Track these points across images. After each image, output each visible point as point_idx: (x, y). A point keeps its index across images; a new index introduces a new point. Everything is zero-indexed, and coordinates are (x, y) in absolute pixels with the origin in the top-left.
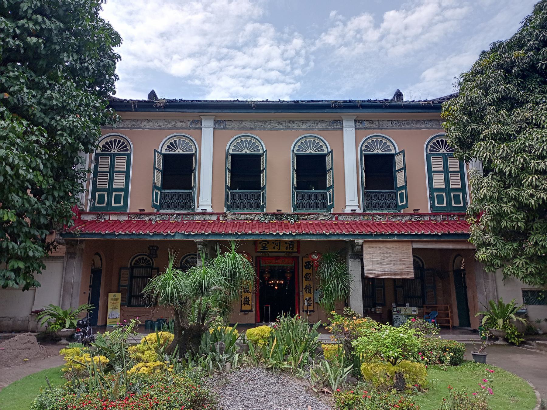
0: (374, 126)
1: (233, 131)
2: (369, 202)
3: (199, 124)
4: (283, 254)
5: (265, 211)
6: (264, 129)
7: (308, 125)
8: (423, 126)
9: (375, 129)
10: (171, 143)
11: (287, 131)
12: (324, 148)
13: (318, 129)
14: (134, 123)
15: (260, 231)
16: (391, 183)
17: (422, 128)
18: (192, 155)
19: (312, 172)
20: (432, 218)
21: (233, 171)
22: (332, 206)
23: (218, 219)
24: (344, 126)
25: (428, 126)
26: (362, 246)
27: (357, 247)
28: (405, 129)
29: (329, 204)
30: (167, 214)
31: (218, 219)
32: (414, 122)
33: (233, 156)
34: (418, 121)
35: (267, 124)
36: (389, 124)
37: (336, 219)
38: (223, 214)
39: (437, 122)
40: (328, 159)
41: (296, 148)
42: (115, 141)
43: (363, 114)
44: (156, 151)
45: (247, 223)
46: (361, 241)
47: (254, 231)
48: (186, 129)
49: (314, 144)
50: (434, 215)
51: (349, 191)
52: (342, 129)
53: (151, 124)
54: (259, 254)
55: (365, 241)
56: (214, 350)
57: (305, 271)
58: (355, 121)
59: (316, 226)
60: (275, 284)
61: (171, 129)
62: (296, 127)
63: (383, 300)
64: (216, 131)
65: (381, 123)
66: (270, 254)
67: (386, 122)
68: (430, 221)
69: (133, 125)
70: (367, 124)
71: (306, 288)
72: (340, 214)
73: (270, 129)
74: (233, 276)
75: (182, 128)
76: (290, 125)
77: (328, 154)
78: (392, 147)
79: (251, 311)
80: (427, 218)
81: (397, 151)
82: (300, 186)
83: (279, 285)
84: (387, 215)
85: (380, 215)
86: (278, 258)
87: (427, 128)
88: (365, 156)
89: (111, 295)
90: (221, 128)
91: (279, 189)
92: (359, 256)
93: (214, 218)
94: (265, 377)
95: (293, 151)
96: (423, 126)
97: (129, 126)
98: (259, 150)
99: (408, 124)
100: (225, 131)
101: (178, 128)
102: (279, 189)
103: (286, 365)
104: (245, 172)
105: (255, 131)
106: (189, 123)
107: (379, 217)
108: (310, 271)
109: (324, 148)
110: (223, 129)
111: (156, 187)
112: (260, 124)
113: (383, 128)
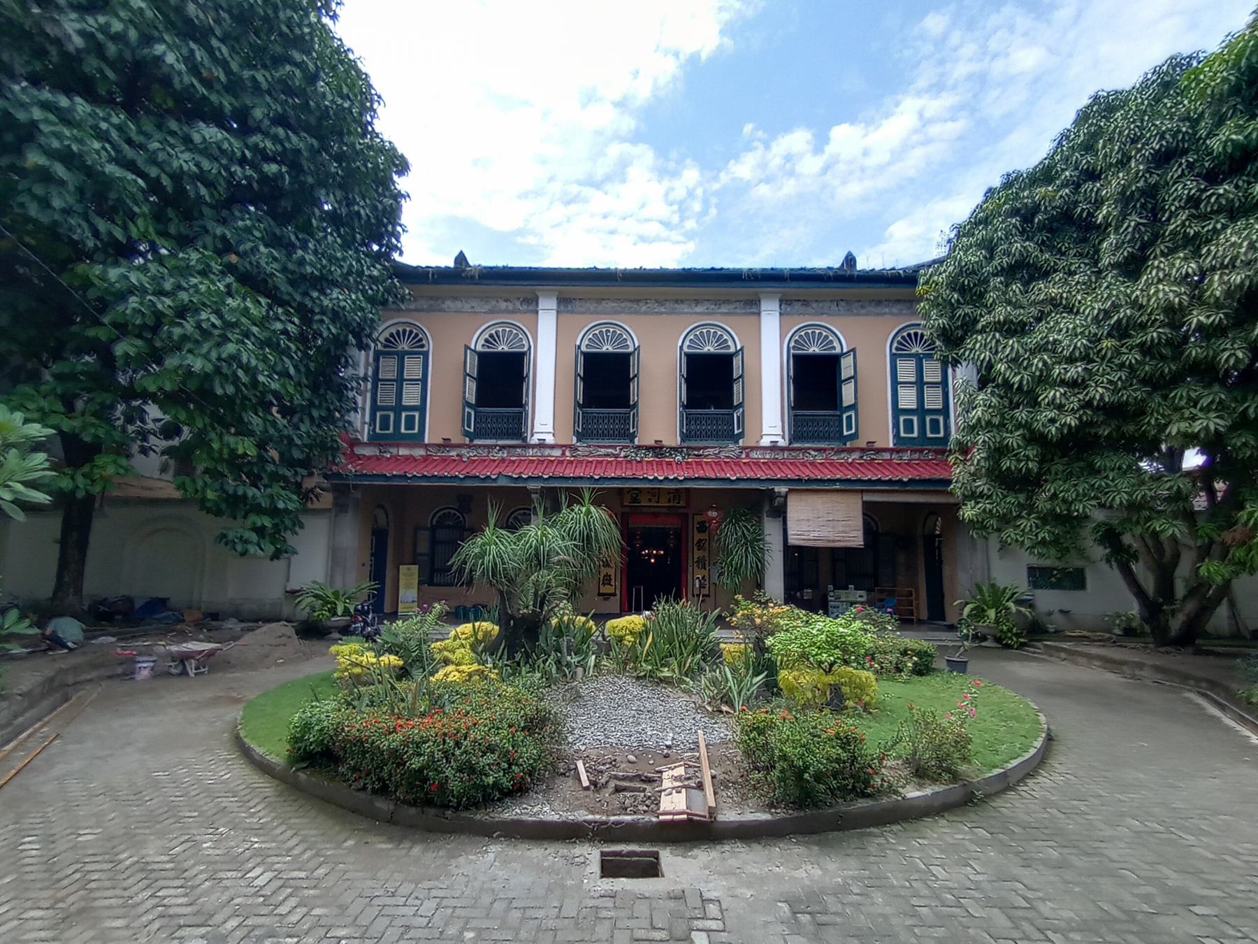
4: (664, 510)
15: (629, 474)
18: (523, 354)
19: (712, 382)
22: (741, 435)
23: (563, 454)
24: (763, 308)
25: (895, 310)
29: (845, 433)
36: (834, 307)
37: (747, 456)
41: (586, 342)
43: (792, 290)
46: (783, 489)
47: (618, 473)
48: (515, 311)
53: (458, 304)
54: (627, 510)
56: (558, 649)
59: (716, 465)
60: (650, 556)
66: (644, 510)
73: (646, 313)
74: (587, 540)
79: (614, 595)
80: (887, 456)
83: (656, 557)
86: (656, 515)
91: (659, 408)
93: (557, 453)
94: (635, 689)
98: (834, 348)
99: (862, 307)
102: (659, 408)
103: (666, 673)
112: (629, 304)
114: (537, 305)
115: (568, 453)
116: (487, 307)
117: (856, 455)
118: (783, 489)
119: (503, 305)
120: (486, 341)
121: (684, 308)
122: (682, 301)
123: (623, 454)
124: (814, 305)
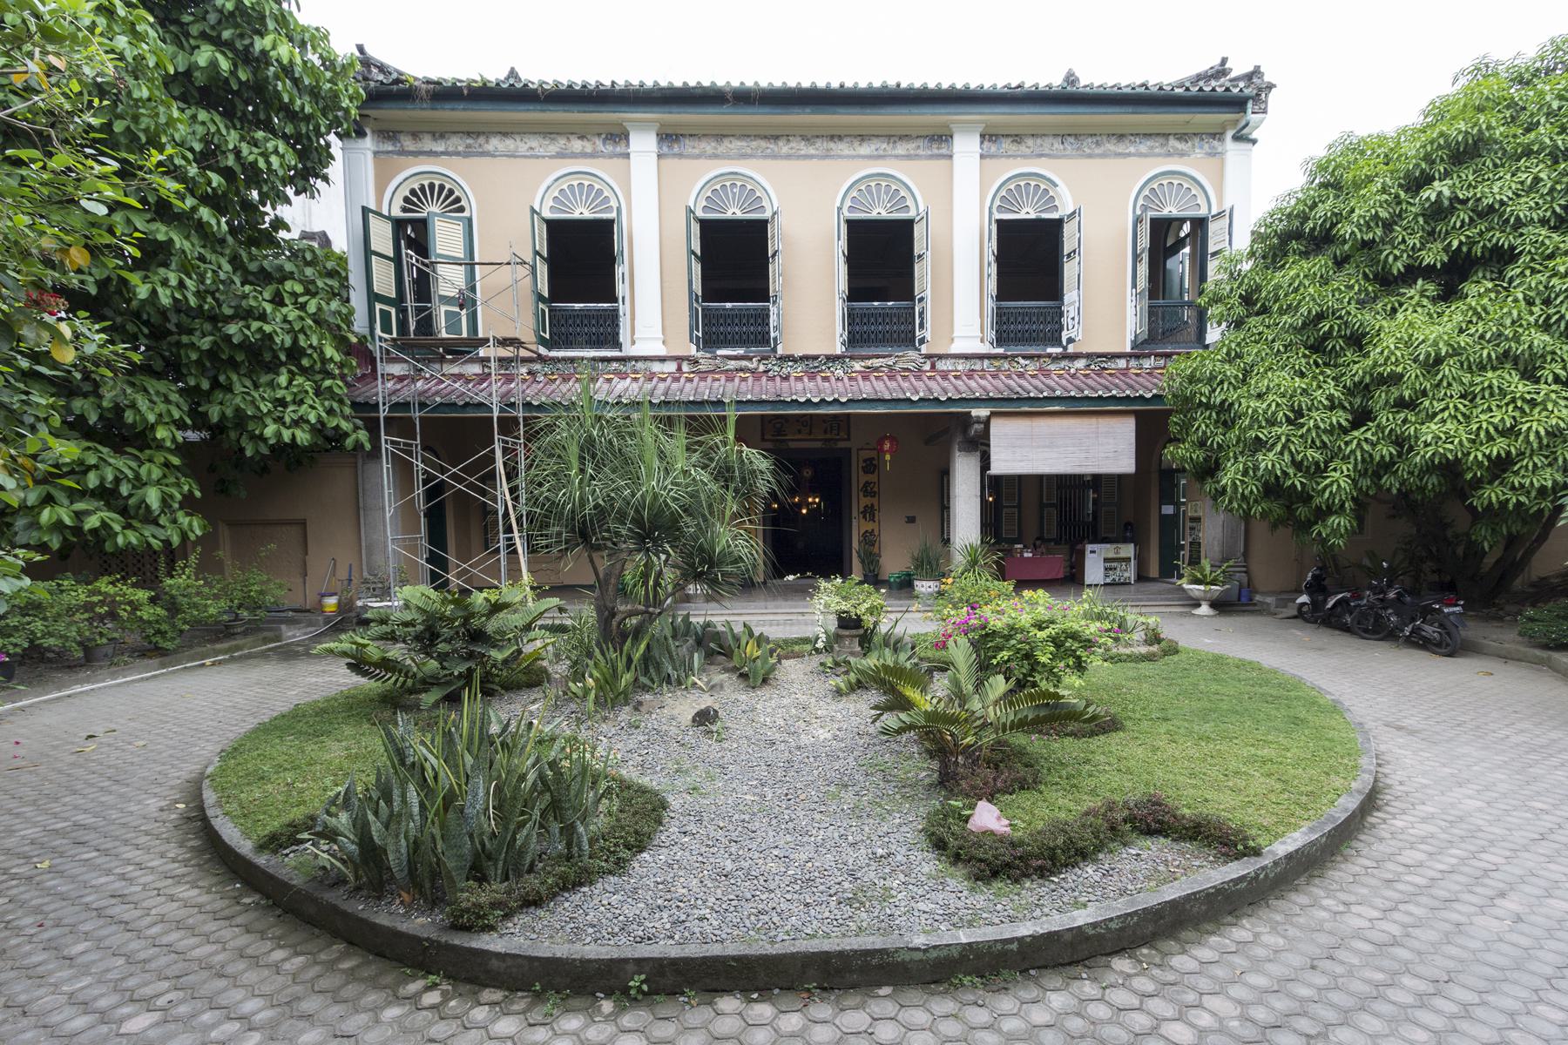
0: (1023, 148)
1: (702, 162)
2: (1009, 330)
3: (623, 143)
5: (780, 351)
6: (774, 157)
7: (873, 147)
8: (1132, 149)
9: (1024, 156)
10: (413, 192)
11: (827, 162)
12: (910, 202)
13: (897, 157)
14: (470, 141)
16: (1052, 288)
17: (1129, 155)
19: (882, 258)
20: (1133, 363)
21: (554, 262)
23: (679, 369)
26: (987, 422)
27: (976, 426)
28: (1090, 156)
30: (564, 359)
31: (679, 369)
32: (1113, 140)
33: (704, 224)
34: (1121, 137)
35: (780, 144)
36: (1057, 145)
37: (933, 366)
38: (687, 358)
39: (1161, 140)
40: (1068, 230)
41: (848, 203)
42: (432, 186)
44: (533, 211)
45: (737, 382)
46: (981, 412)
48: (593, 155)
49: (886, 193)
50: (1137, 357)
51: (958, 301)
52: (951, 157)
55: (993, 414)
57: (864, 478)
58: (982, 136)
61: (561, 155)
62: (846, 152)
63: (1047, 526)
64: (663, 162)
65: (1039, 141)
67: (1050, 140)
68: (1128, 369)
69: (469, 146)
70: (1006, 145)
71: (864, 513)
72: (940, 357)
73: (788, 157)
75: (584, 155)
76: (832, 145)
77: (1220, 215)
78: (1201, 200)
80: (1122, 363)
81: (1214, 212)
82: (854, 294)
84: (1039, 357)
85: (1024, 357)
87: (1141, 155)
88: (999, 222)
89: (1125, 430)
90: (675, 155)
91: (810, 298)
92: (980, 445)
95: (840, 209)
96: (1132, 149)
97: (460, 149)
100: (684, 162)
101: (574, 156)
102: (810, 298)
104: (733, 260)
105: (753, 162)
106: (599, 143)
107: (1022, 361)
108: (872, 478)
109: (1201, 200)
110: (680, 156)
111: (540, 298)
112: (763, 143)
113: (1041, 156)
114: (628, 145)
115: (685, 368)
116: (553, 148)
117: (1080, 364)
118: (981, 412)
119: (577, 145)
120: (406, 200)
121: (842, 148)
122: (840, 138)
123: (762, 368)
124: (1030, 142)
